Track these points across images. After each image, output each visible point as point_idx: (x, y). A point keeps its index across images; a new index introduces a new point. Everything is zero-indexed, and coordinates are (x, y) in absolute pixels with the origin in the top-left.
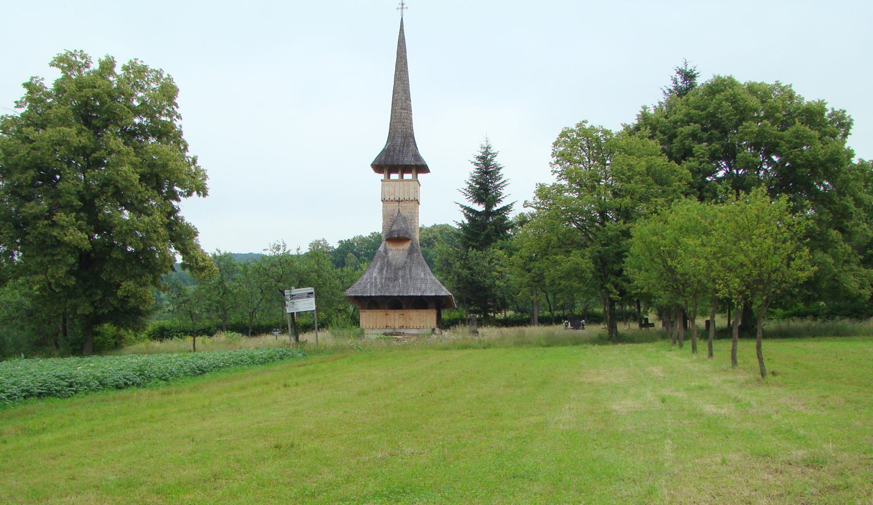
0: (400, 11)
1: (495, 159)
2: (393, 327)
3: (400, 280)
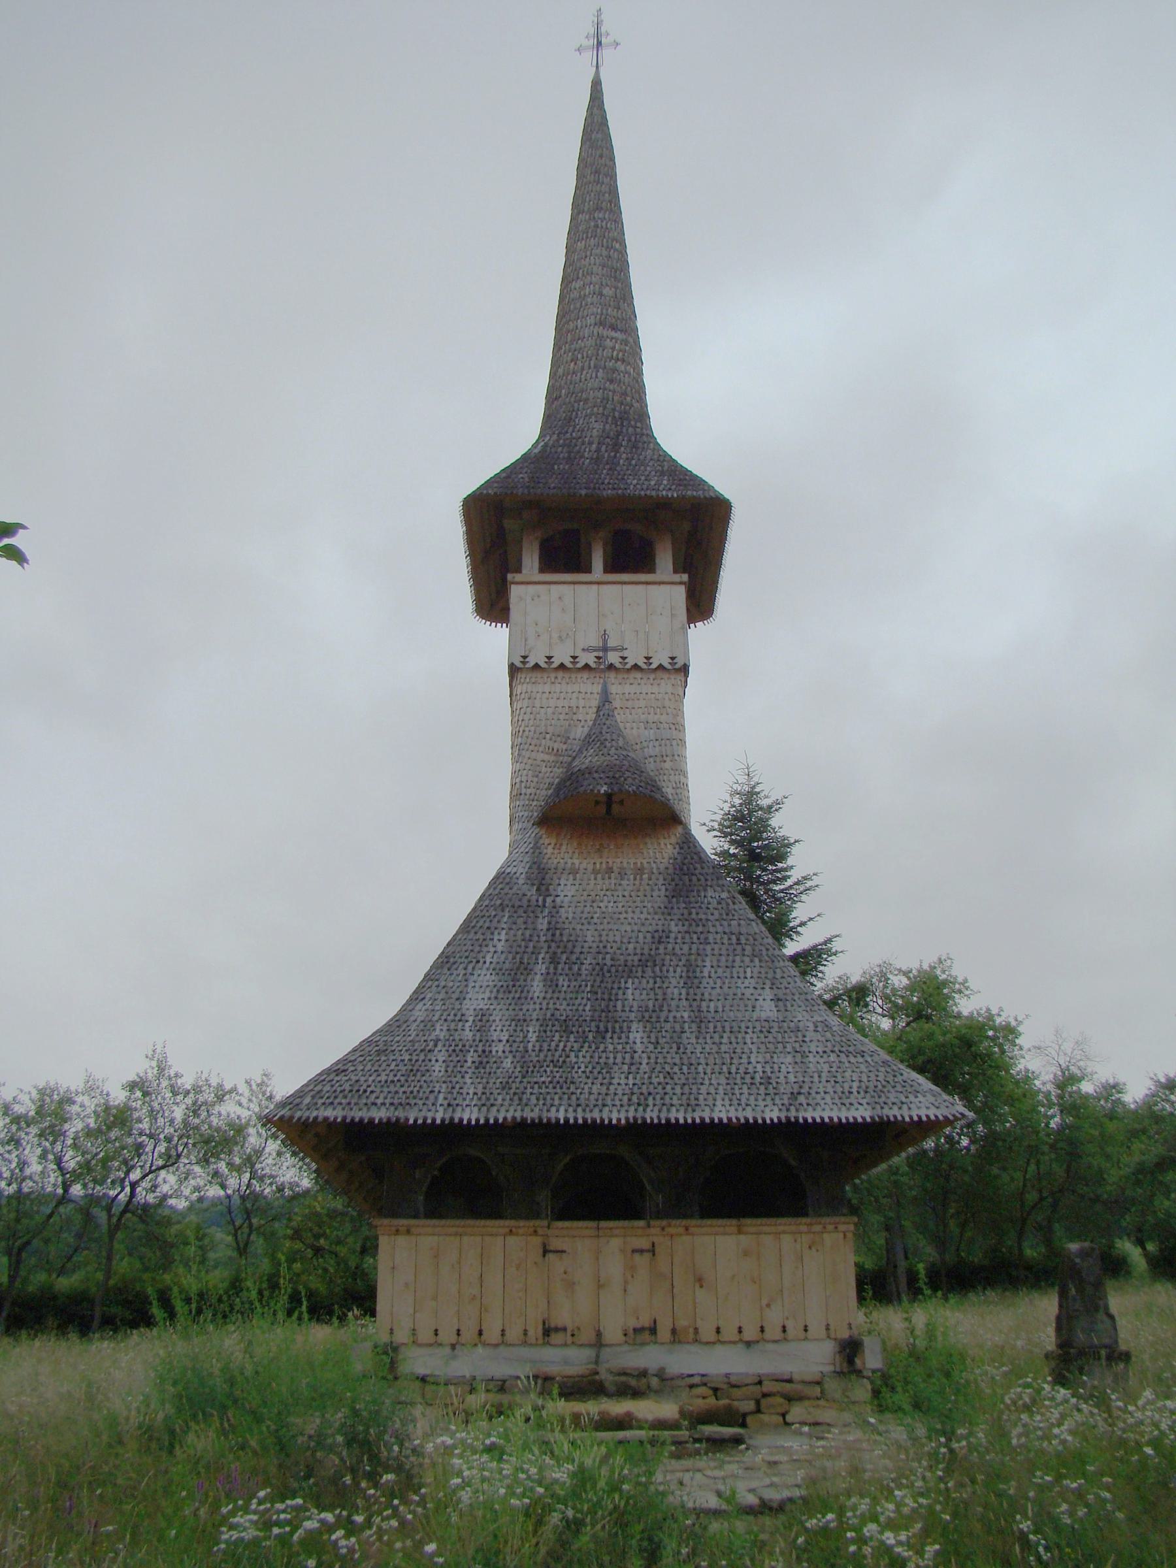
0: (589, 56)
2: (587, 1336)
3: (637, 1035)
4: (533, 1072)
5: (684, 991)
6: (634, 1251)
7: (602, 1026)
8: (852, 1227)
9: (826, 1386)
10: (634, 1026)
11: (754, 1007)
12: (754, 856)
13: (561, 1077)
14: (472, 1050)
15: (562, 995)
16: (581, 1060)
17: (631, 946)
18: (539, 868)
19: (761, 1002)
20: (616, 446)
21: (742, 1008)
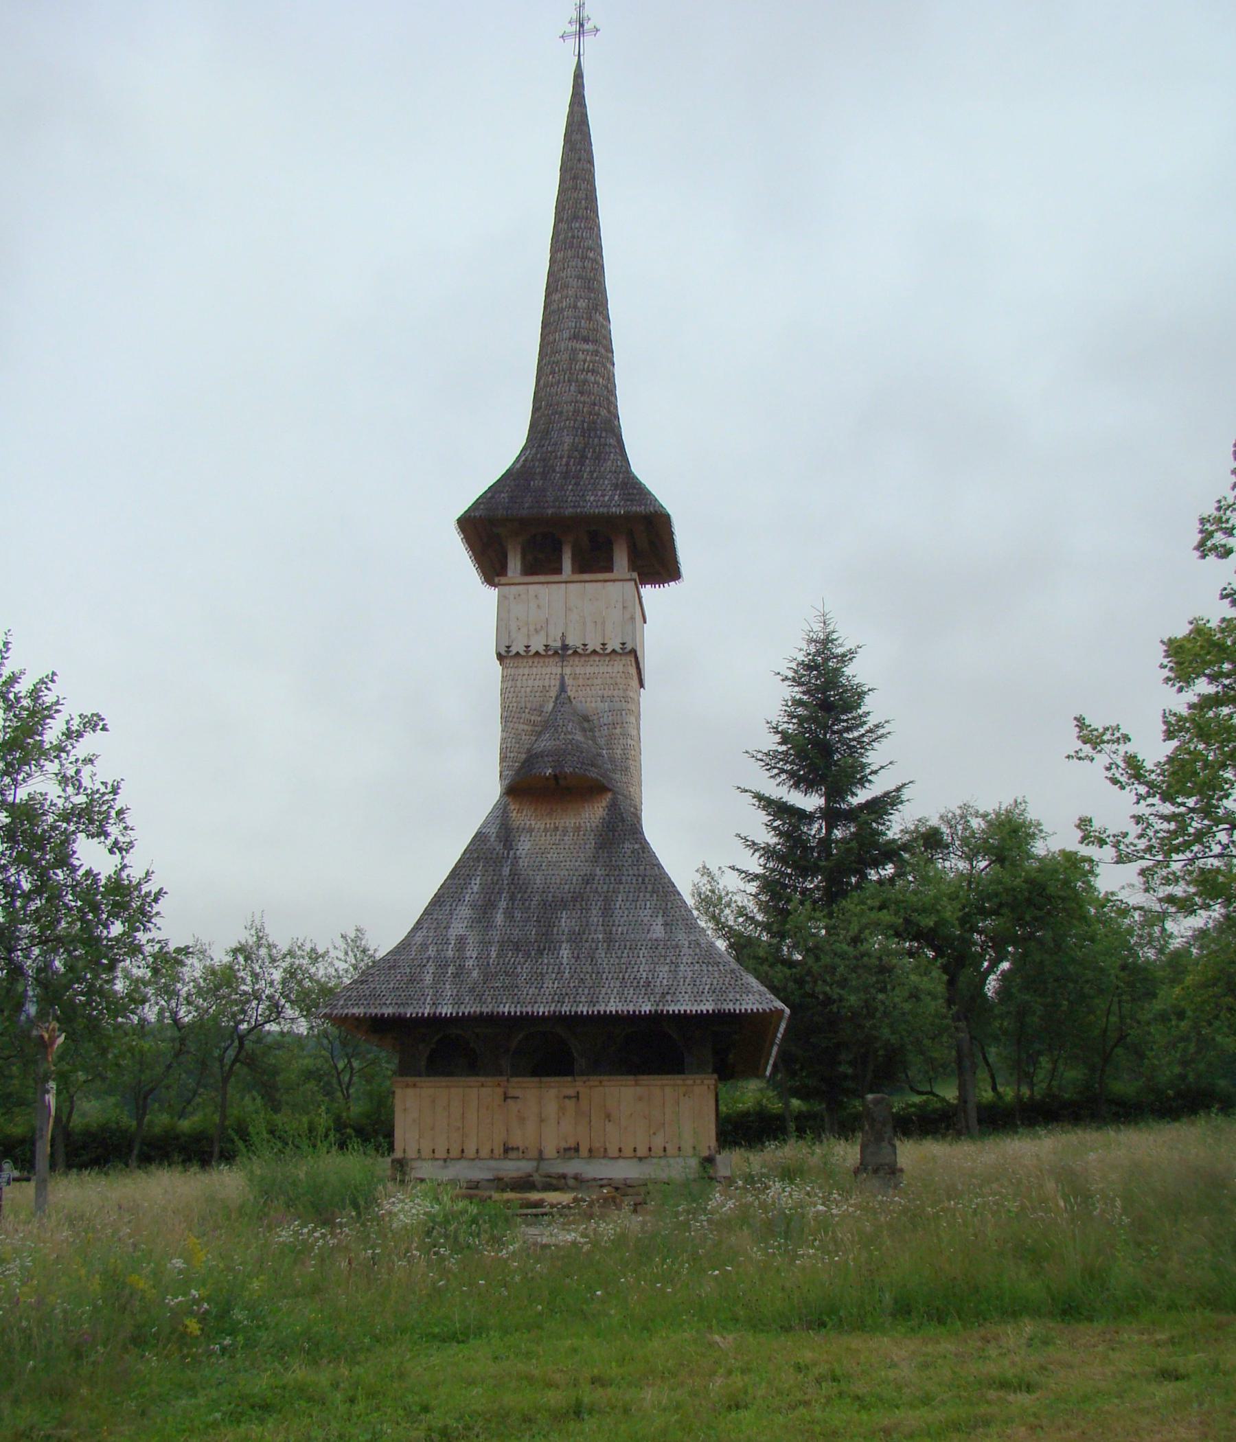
0: (571, 43)
1: (848, 671)
2: (534, 1154)
3: (565, 952)
5: (601, 919)
6: (565, 1097)
7: (542, 945)
8: (713, 1082)
10: (564, 945)
11: (649, 930)
12: (826, 706)
15: (516, 924)
16: (524, 970)
17: (567, 887)
18: (506, 828)
19: (654, 926)
20: (582, 460)
21: (640, 931)
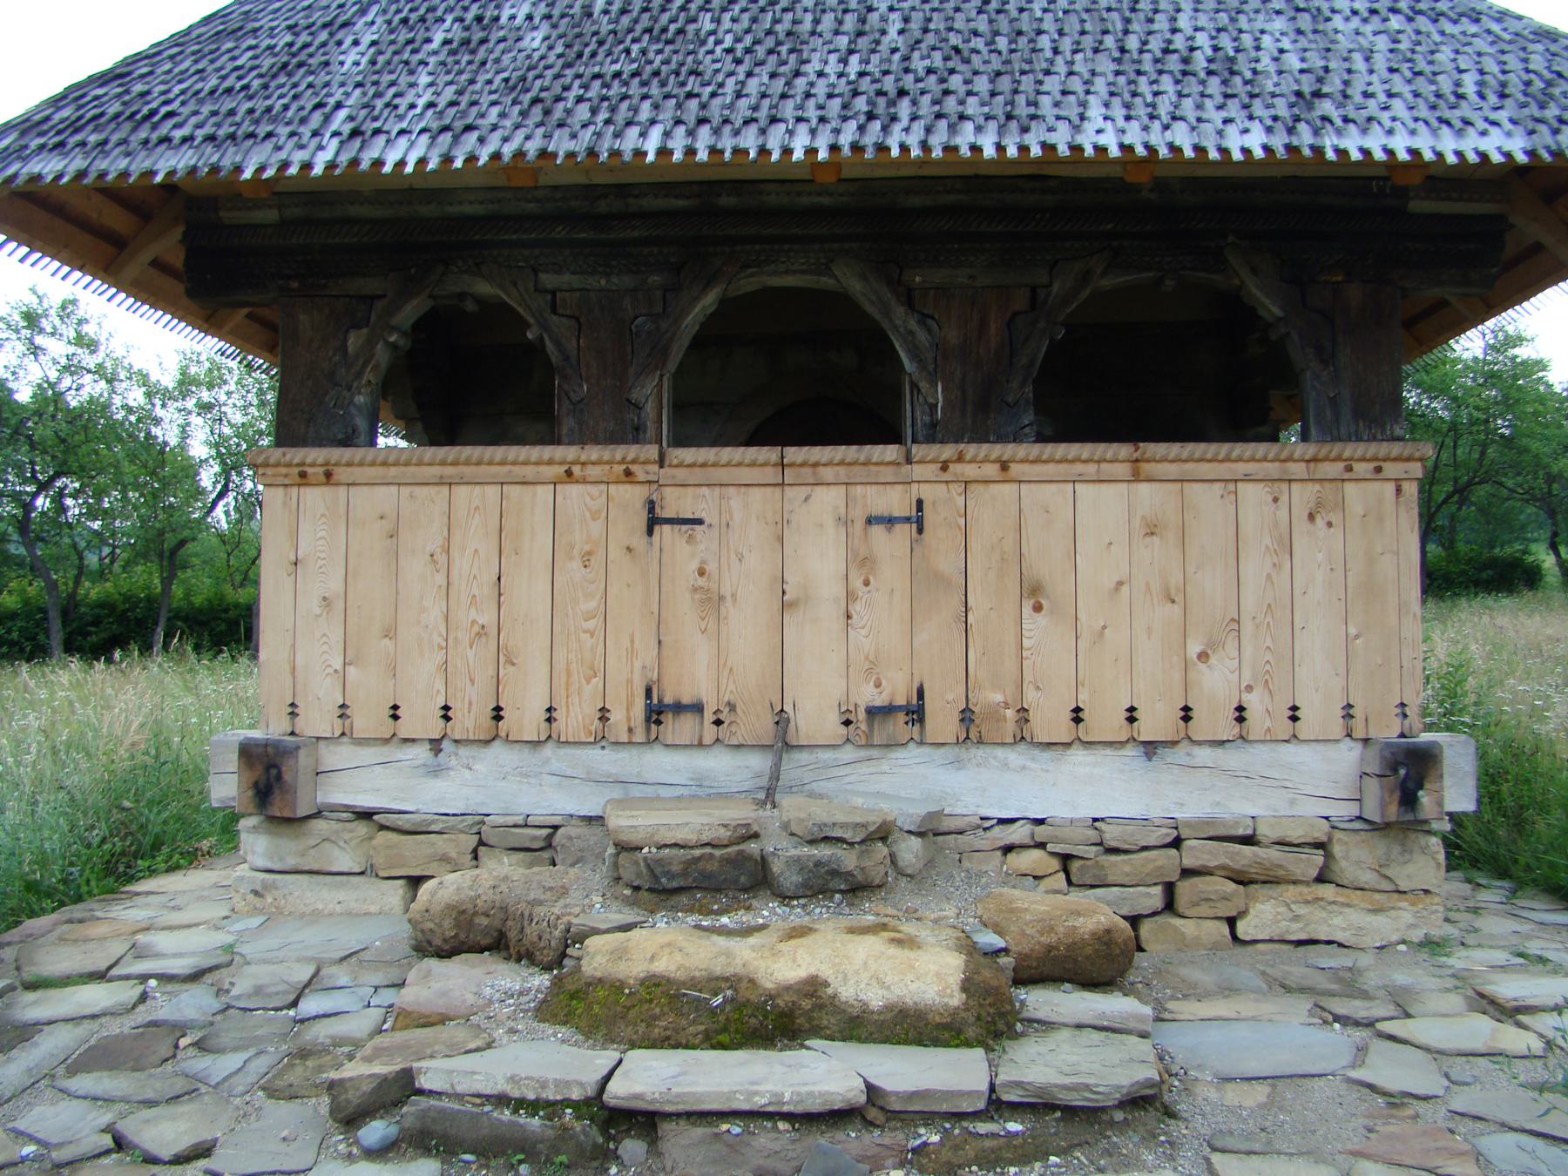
2: (755, 723)
4: (594, 55)
6: (870, 521)
9: (1337, 850)
13: (666, 62)
14: (449, 18)
